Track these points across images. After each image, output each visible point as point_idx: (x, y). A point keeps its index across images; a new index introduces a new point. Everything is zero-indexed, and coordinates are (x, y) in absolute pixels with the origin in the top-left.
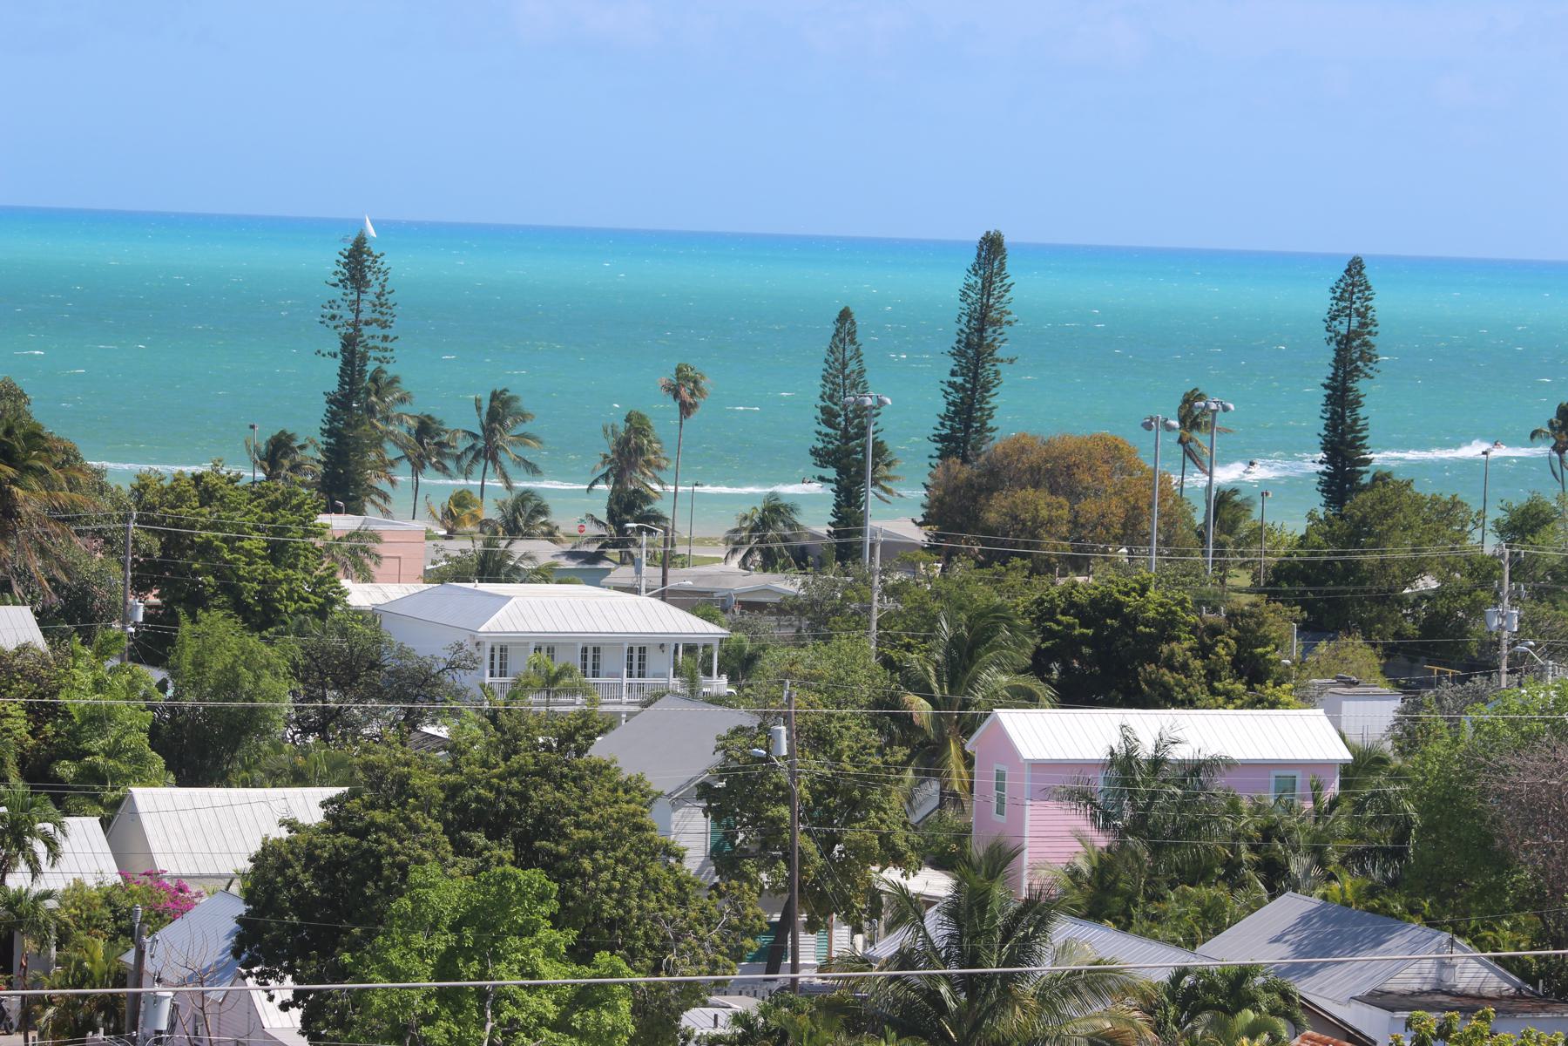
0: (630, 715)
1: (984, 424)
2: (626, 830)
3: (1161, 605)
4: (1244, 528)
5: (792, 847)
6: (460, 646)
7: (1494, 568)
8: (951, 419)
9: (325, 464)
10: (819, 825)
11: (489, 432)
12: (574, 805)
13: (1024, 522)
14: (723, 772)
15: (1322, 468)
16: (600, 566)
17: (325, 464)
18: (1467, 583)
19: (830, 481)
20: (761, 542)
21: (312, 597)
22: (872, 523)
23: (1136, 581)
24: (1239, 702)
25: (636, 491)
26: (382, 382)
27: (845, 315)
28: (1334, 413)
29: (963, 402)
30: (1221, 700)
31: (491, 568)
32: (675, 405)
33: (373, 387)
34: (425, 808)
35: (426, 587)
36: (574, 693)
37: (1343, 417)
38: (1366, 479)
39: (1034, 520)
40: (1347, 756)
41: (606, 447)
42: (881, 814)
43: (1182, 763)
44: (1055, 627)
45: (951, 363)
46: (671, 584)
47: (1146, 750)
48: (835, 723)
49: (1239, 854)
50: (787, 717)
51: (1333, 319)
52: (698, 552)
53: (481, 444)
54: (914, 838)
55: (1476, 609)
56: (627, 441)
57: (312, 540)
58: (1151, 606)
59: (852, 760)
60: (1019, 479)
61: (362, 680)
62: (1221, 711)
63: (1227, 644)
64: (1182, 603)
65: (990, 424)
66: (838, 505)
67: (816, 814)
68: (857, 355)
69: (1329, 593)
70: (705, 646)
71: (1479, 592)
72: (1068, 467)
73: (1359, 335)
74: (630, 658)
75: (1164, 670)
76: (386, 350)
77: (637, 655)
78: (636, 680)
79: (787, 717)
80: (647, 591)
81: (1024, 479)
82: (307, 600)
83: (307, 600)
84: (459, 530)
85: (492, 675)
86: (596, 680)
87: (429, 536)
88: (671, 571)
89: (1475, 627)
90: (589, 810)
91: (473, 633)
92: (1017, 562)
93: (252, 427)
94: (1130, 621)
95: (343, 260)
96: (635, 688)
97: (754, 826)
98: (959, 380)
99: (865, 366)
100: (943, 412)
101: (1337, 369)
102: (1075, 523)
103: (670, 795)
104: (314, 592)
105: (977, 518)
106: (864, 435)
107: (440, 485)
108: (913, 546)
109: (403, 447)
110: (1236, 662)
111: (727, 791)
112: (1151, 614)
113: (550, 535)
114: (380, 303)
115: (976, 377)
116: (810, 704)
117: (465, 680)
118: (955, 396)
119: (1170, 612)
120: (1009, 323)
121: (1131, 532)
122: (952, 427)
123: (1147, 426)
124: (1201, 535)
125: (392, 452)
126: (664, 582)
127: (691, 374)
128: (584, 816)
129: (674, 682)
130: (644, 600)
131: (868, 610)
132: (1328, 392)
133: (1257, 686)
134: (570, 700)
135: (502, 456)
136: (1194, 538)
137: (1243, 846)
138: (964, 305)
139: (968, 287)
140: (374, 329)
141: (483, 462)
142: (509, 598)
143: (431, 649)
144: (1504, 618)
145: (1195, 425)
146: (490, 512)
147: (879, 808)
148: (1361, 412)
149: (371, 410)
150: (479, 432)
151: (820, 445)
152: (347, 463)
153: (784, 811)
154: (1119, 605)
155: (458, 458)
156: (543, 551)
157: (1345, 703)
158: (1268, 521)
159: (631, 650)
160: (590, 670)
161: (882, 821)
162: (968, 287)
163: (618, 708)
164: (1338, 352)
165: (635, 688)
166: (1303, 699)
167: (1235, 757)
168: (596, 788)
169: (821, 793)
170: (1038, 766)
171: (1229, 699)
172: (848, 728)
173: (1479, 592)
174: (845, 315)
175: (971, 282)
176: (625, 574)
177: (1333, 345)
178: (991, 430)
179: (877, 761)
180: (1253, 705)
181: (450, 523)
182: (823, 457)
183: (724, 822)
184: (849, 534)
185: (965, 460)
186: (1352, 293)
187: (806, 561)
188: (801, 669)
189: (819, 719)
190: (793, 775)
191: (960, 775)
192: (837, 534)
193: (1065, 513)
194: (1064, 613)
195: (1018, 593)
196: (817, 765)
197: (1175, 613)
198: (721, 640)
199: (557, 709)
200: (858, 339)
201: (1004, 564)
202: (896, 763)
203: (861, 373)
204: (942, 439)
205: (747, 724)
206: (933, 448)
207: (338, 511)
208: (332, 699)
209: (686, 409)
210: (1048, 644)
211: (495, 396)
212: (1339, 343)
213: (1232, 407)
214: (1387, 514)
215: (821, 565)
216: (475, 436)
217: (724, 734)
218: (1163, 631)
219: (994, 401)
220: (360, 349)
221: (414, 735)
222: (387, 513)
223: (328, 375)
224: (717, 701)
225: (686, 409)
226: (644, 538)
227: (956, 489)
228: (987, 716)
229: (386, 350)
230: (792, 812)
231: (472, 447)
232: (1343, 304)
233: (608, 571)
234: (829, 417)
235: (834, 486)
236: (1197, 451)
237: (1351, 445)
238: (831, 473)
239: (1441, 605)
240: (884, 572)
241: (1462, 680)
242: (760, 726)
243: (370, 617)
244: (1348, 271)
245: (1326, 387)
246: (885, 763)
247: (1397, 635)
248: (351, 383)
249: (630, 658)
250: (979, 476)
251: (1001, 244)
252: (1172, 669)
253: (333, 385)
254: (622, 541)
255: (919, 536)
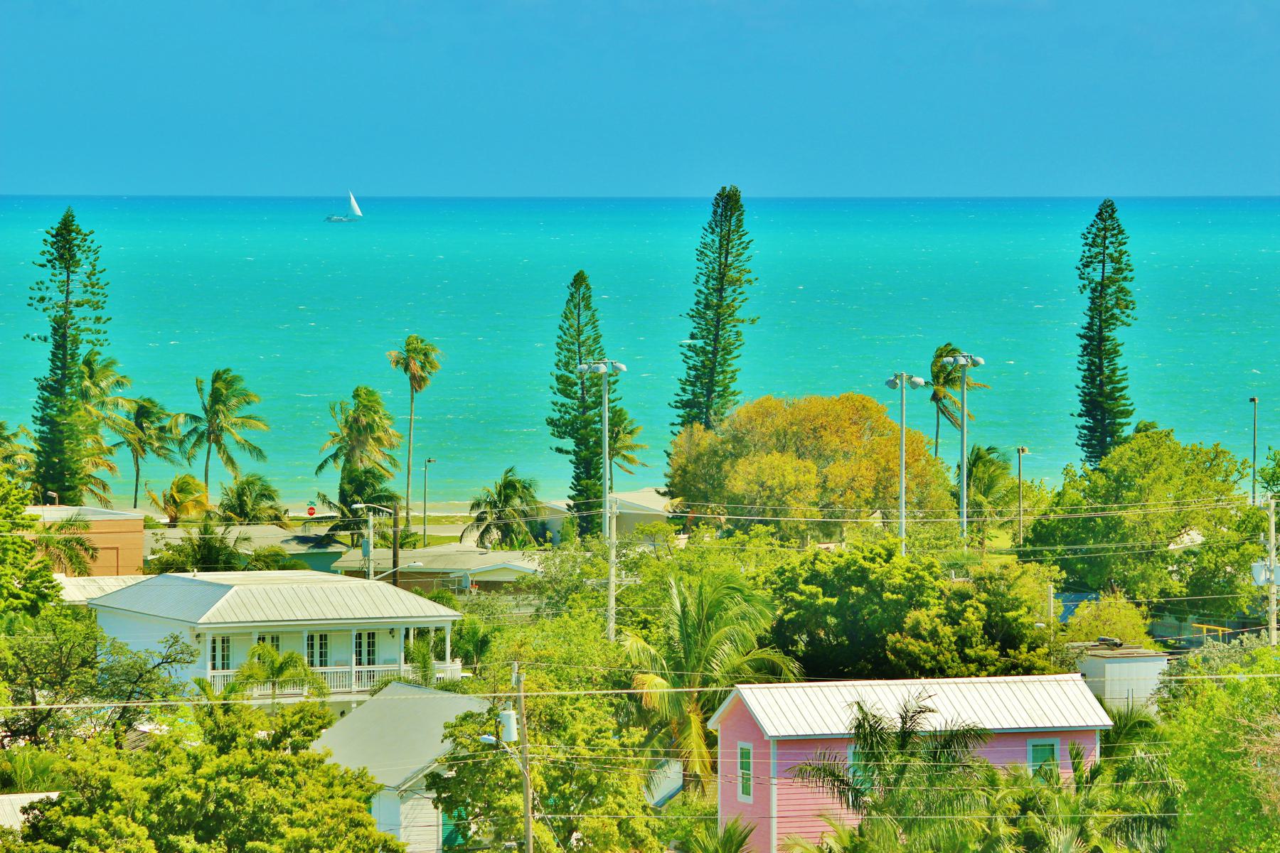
0: (359, 703)
1: (726, 388)
2: (343, 827)
3: (908, 570)
4: (1001, 487)
5: (526, 837)
6: (176, 639)
7: (1262, 519)
8: (693, 384)
9: (38, 453)
10: (555, 812)
11: (212, 412)
12: (286, 802)
13: (772, 490)
14: (453, 760)
15: (1082, 421)
16: (330, 549)
17: (38, 453)
18: (1235, 537)
19: (568, 452)
20: (499, 518)
21: (23, 594)
22: (609, 497)
23: (883, 547)
24: (992, 669)
25: (367, 472)
26: (96, 367)
27: (579, 280)
28: (1091, 363)
29: (704, 366)
30: (973, 667)
31: (211, 557)
32: (406, 378)
33: (85, 369)
34: (129, 813)
35: (143, 578)
36: (302, 683)
37: (1100, 368)
38: (1128, 431)
39: (781, 486)
40: (1108, 722)
41: (337, 426)
42: (620, 799)
43: (934, 735)
44: (798, 597)
45: (690, 326)
46: (402, 566)
47: (892, 721)
48: (567, 708)
49: (997, 829)
50: (516, 701)
51: (1086, 266)
52: (432, 530)
53: (203, 427)
54: (654, 822)
55: (1243, 564)
56: (356, 420)
57: (20, 533)
58: (896, 572)
59: (588, 743)
60: (765, 444)
61: (73, 678)
62: (974, 679)
63: (977, 608)
64: (930, 567)
65: (733, 387)
66: (577, 478)
67: (551, 802)
68: (593, 322)
69: (1089, 551)
70: (437, 630)
71: (1247, 544)
72: (815, 430)
73: (1114, 282)
74: (359, 645)
75: (909, 639)
76: (98, 332)
77: (366, 642)
78: (365, 668)
79: (516, 701)
80: (376, 574)
81: (770, 443)
82: (17, 597)
83: (17, 597)
84: (183, 517)
85: (214, 668)
86: (323, 669)
87: (148, 524)
88: (401, 553)
89: (1242, 581)
90: (303, 807)
91: (192, 624)
92: (760, 528)
93: (1253, 400)
94: (876, 589)
95: (51, 239)
96: (365, 676)
97: (486, 815)
98: (700, 343)
99: (601, 332)
100: (684, 377)
101: (1092, 318)
102: (823, 487)
103: (397, 788)
104: (25, 588)
105: (721, 486)
106: (600, 404)
107: (161, 474)
108: (651, 517)
109: (121, 433)
110: (989, 627)
111: (458, 781)
112: (898, 580)
113: (276, 519)
114: (92, 281)
115: (716, 340)
116: (541, 687)
117: (185, 675)
118: (696, 360)
119: (918, 577)
120: (750, 282)
121: (881, 497)
122: (693, 393)
123: (892, 384)
124: (956, 496)
125: (108, 437)
126: (395, 564)
127: (421, 346)
128: (298, 813)
129: (406, 670)
130: (372, 584)
131: (606, 586)
132: (1086, 342)
133: (1011, 652)
134: (297, 691)
135: (226, 439)
136: (948, 499)
137: (1000, 818)
138: (702, 265)
139: (705, 245)
140: (86, 311)
141: (205, 446)
142: (231, 587)
143: (138, 643)
144: (1271, 571)
145: (949, 381)
146: (214, 500)
147: (617, 792)
148: (1120, 362)
149: (85, 395)
150: (202, 414)
151: (556, 416)
152: (62, 452)
153: (516, 799)
154: (864, 571)
155: (181, 442)
156: (263, 537)
157: (1108, 666)
158: (1027, 479)
159: (359, 636)
160: (317, 659)
161: (621, 806)
162: (705, 245)
163: (347, 698)
164: (1093, 300)
165: (365, 676)
166: (1062, 662)
167: (988, 727)
168: (310, 783)
169: (556, 779)
170: (786, 743)
171: (982, 667)
172: (582, 710)
173: (1247, 544)
174: (579, 280)
175: (708, 240)
176: (353, 558)
177: (1088, 293)
178: (733, 394)
179: (614, 743)
180: (1006, 671)
181: (172, 509)
182: (559, 427)
183: (455, 813)
184: (589, 507)
185: (708, 426)
186: (1105, 238)
187: (544, 536)
188: (528, 650)
189: (550, 702)
190: (525, 761)
191: (701, 756)
192: (577, 507)
193: (813, 478)
194: (806, 582)
195: (756, 560)
196: (548, 751)
197: (922, 578)
198: (454, 623)
199: (283, 701)
200: (593, 305)
201: (746, 533)
202: (633, 745)
203: (596, 340)
204: (685, 405)
205: (476, 710)
206: (675, 415)
207: (48, 501)
208: (43, 699)
209: (417, 382)
210: (791, 615)
211: (217, 377)
212: (1094, 290)
213: (982, 361)
214: (1147, 467)
215: (559, 541)
216: (195, 418)
217: (453, 721)
218: (911, 597)
219: (735, 364)
220: (70, 332)
221: (131, 735)
222: (105, 503)
223: (40, 362)
224: (450, 687)
225: (417, 382)
226: (372, 519)
227: (698, 458)
228: (727, 693)
229: (98, 332)
230: (526, 800)
231: (195, 430)
232: (1097, 250)
233: (339, 554)
234: (565, 386)
235: (573, 458)
236: (951, 408)
237: (1110, 396)
238: (569, 444)
239: (1208, 560)
240: (622, 545)
241: (1227, 639)
242: (490, 711)
243: (84, 611)
244: (1099, 215)
245: (1082, 337)
246: (622, 745)
247: (1163, 593)
248: (64, 367)
249: (359, 645)
250: (723, 442)
251: (737, 201)
252: (918, 636)
253: (44, 369)
254: (352, 523)
255: (663, 506)
